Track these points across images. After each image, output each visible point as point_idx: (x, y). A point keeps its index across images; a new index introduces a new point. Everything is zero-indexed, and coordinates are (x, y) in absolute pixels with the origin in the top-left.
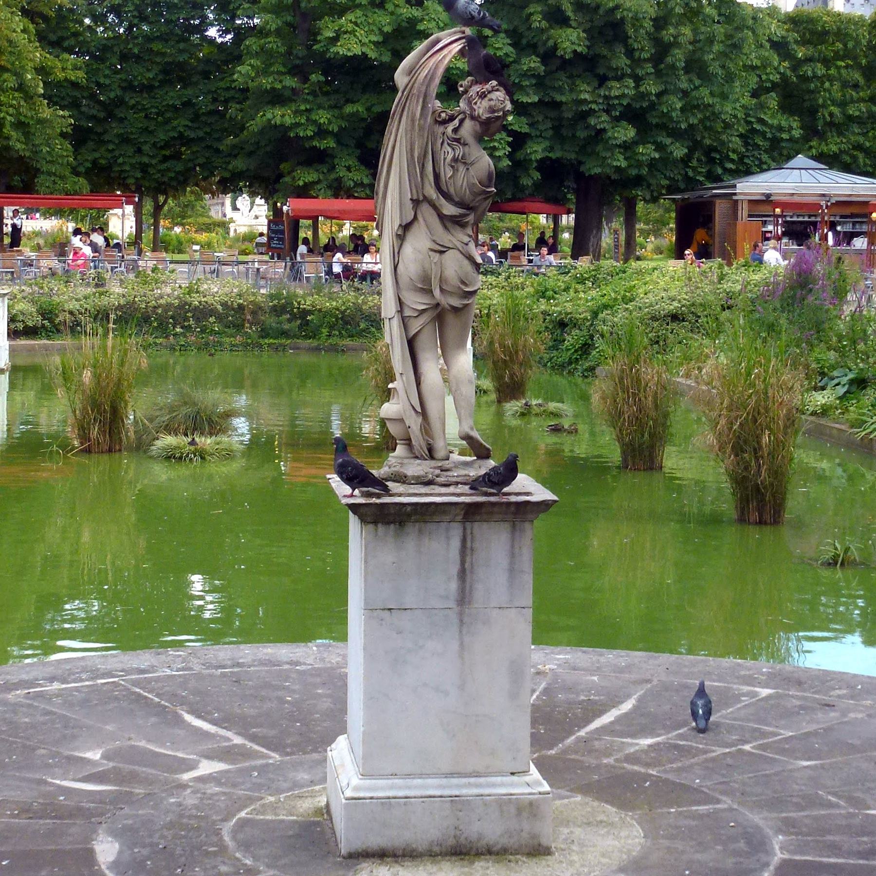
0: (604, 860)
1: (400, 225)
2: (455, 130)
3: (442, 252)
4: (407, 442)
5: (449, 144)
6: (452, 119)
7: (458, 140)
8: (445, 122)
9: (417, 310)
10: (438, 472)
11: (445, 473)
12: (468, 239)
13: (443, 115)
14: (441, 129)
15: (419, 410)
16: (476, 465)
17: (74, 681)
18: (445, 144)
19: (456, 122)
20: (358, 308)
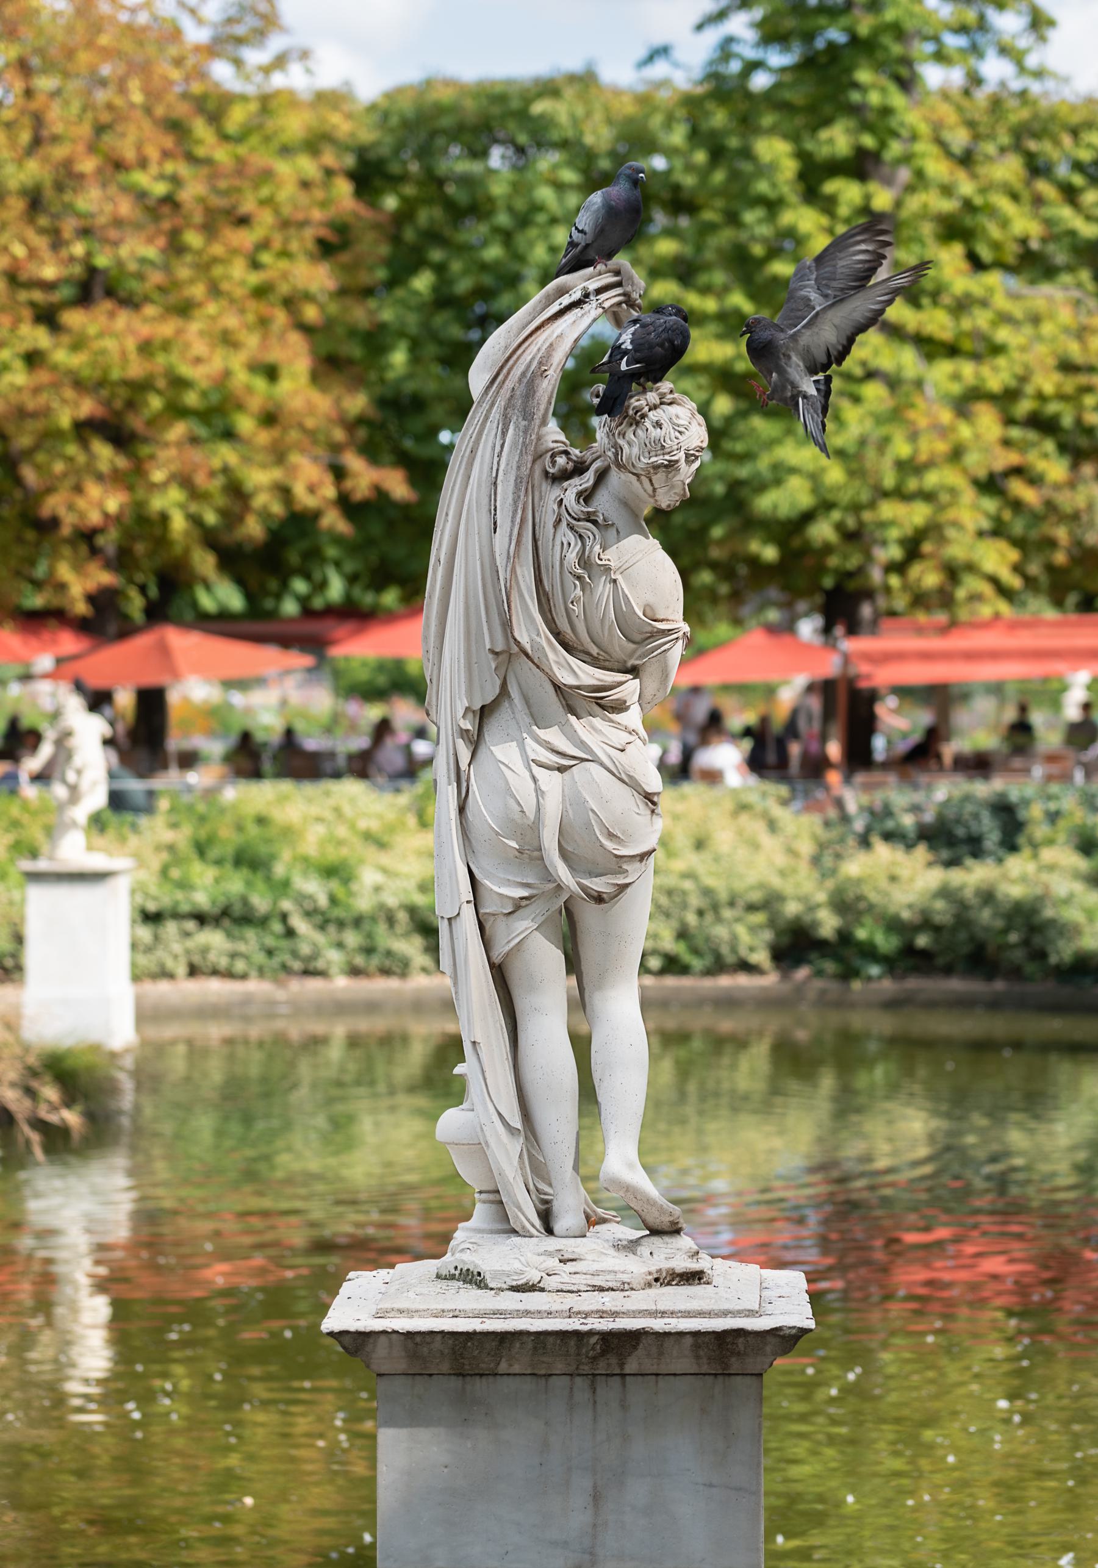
0: (253, 830)
1: (467, 709)
2: (586, 496)
3: (561, 769)
4: (491, 1197)
5: (571, 528)
6: (580, 469)
7: (590, 518)
8: (564, 476)
9: (618, 885)
10: (553, 1263)
11: (570, 1267)
12: (625, 737)
13: (561, 460)
14: (555, 493)
15: (517, 1122)
16: (644, 1250)
17: (501, 594)
18: (564, 524)
19: (588, 479)
20: (971, 778)
